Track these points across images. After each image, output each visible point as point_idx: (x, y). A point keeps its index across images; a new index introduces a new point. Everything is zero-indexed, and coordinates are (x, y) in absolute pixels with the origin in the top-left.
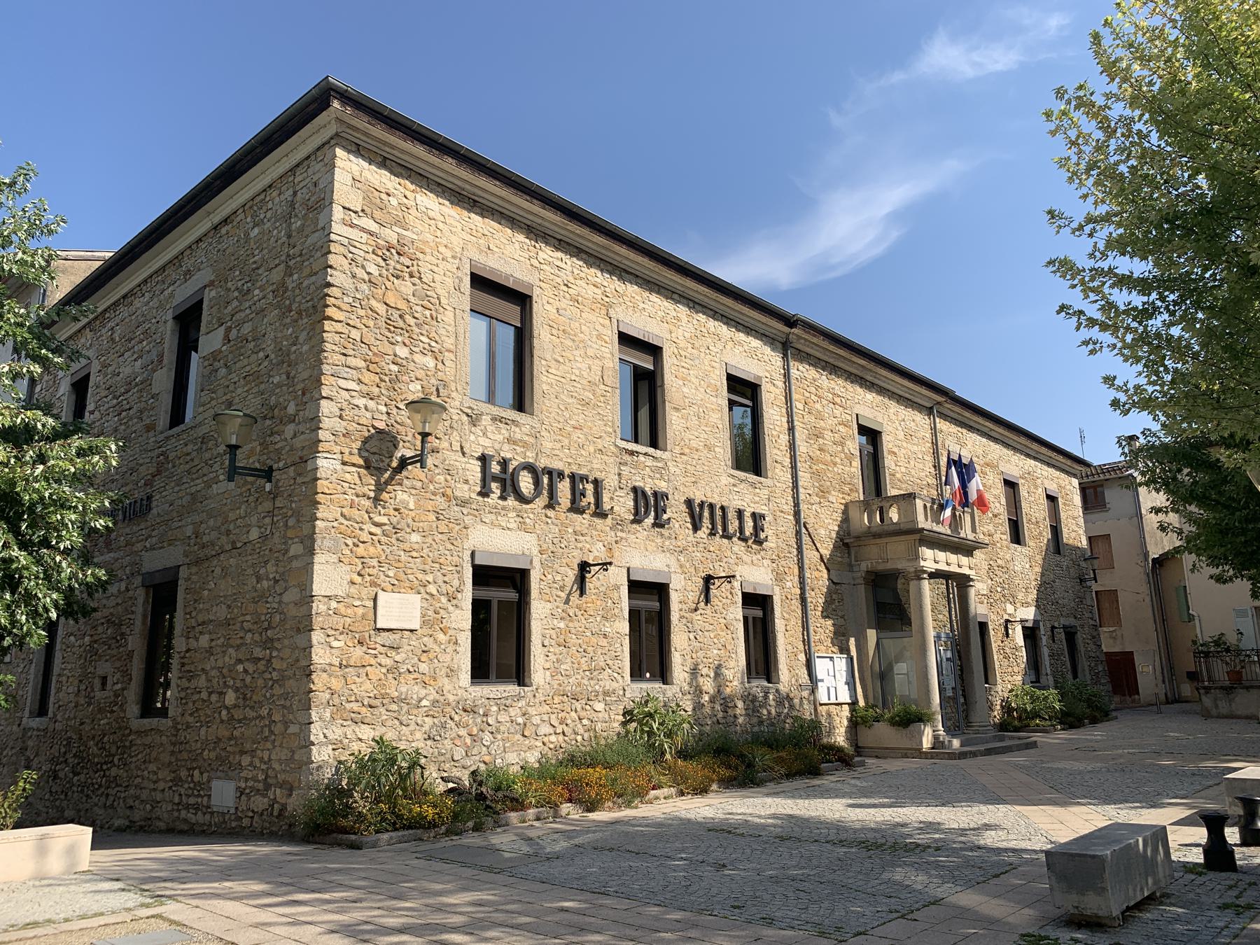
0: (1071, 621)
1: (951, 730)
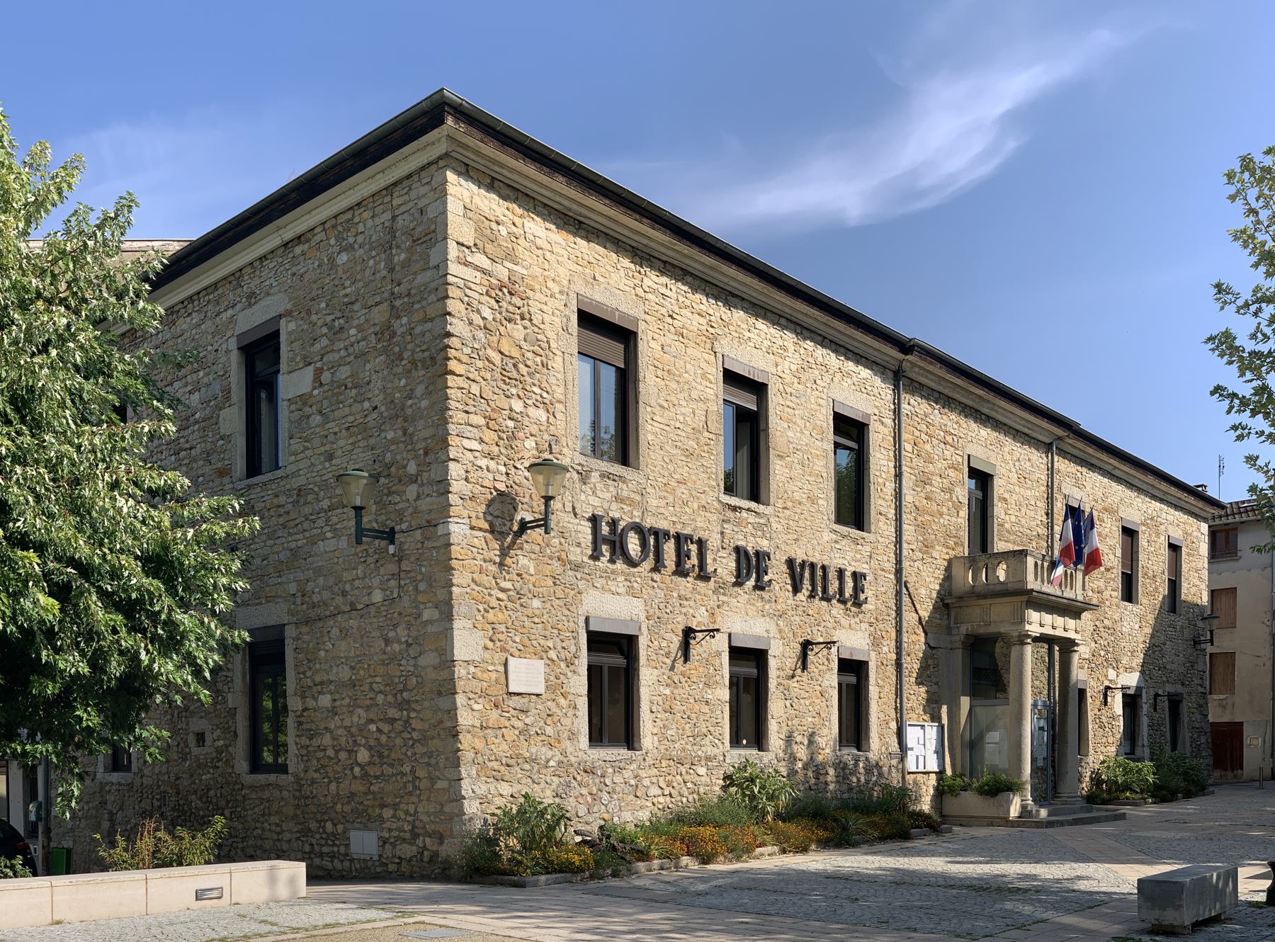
0: (1178, 688)
1: (1040, 799)
